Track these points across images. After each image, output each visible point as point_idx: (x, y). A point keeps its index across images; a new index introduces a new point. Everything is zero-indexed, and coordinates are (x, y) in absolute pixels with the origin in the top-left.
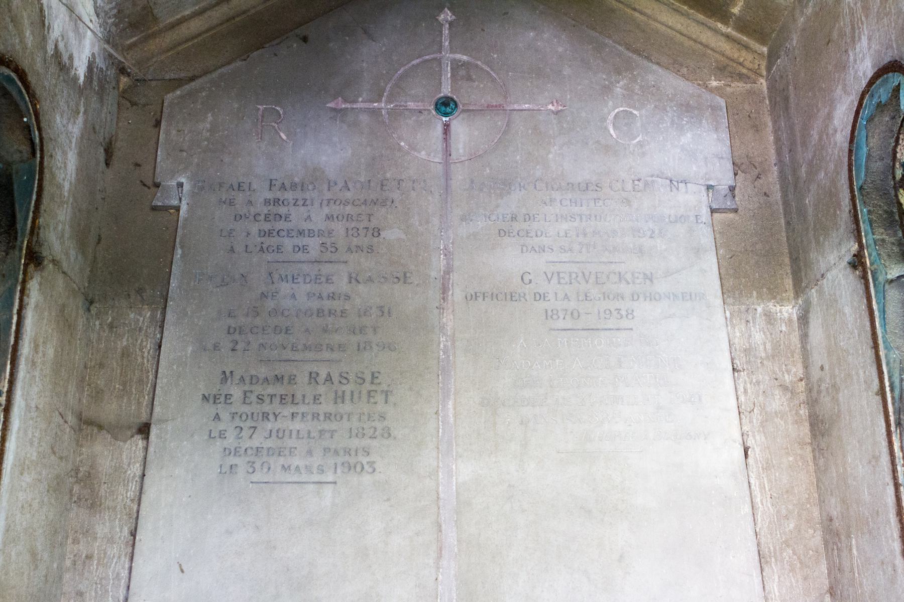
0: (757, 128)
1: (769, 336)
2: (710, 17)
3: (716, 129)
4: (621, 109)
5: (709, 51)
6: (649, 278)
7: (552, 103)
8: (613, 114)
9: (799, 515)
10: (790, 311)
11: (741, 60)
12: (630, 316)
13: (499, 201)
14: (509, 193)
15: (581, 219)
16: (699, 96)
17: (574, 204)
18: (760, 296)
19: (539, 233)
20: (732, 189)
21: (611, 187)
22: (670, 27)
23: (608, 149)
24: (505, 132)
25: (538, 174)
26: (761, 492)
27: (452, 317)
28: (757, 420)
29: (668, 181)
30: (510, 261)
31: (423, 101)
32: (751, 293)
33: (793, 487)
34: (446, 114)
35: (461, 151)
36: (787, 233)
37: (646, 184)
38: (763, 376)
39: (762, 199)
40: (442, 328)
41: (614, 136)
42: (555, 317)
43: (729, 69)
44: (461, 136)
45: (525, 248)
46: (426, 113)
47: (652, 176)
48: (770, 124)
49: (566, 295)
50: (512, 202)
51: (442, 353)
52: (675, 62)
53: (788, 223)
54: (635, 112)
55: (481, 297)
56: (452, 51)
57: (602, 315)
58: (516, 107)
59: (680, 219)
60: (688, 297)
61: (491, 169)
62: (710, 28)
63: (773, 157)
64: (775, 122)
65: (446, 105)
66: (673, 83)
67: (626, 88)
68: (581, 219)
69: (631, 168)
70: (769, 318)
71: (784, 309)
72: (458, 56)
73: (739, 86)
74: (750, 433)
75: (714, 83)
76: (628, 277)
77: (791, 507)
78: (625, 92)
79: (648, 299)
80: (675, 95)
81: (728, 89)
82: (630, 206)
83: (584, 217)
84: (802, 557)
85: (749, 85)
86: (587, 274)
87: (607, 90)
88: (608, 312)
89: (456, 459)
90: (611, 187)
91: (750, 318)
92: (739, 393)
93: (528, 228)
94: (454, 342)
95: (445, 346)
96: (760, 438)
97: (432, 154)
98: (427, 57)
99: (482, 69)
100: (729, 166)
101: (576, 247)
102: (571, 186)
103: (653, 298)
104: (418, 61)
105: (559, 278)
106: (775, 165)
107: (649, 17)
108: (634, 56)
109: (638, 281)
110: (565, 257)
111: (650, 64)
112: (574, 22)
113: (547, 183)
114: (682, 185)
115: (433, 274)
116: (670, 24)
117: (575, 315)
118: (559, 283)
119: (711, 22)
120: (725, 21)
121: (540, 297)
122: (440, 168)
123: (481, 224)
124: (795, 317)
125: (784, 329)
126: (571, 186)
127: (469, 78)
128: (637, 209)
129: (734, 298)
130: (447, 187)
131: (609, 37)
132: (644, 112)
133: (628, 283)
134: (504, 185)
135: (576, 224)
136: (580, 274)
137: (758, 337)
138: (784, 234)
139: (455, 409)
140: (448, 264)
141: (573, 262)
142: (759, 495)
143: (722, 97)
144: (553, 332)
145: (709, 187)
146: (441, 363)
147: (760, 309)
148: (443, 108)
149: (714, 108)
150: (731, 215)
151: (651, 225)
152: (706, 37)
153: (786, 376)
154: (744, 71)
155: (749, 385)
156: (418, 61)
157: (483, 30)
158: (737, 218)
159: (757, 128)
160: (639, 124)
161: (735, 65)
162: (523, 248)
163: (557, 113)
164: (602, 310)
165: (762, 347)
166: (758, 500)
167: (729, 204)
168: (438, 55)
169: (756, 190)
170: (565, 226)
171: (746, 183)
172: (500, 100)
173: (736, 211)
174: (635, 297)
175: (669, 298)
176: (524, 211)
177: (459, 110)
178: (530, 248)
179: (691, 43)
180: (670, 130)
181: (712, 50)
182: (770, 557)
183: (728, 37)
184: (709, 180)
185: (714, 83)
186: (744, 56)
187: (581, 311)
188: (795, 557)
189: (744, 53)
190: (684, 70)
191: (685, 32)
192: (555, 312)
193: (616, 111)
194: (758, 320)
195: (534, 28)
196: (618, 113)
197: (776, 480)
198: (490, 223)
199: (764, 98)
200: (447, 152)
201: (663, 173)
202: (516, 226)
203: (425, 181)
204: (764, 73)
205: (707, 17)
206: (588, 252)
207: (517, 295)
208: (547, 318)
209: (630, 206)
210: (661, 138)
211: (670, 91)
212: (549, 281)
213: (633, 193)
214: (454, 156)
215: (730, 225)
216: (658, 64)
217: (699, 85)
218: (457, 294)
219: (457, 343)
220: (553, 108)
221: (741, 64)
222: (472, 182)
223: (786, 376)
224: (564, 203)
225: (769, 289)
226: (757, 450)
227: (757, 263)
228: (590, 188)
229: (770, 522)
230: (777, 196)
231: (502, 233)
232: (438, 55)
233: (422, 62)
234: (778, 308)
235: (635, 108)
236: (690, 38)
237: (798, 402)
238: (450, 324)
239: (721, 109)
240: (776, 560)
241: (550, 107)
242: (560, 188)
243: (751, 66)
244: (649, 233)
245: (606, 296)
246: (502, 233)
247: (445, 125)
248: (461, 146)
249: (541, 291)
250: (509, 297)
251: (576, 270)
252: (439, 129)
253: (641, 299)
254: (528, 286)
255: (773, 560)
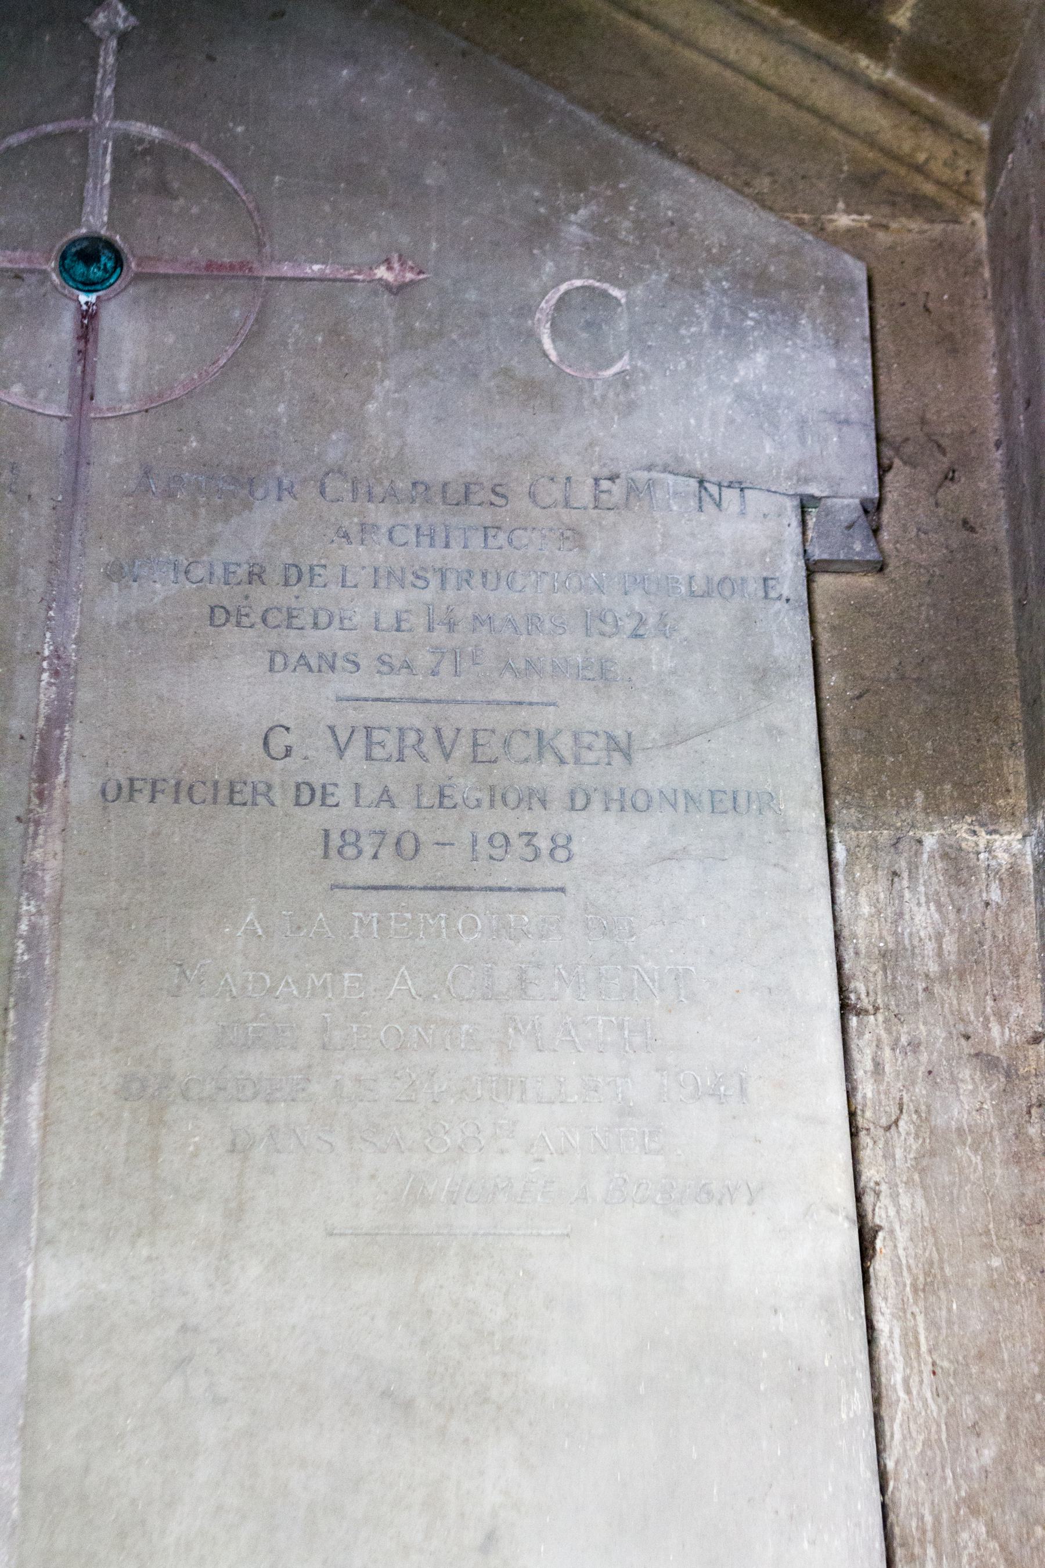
0: (952, 344)
1: (952, 916)
2: (839, 39)
3: (837, 344)
4: (578, 283)
5: (834, 133)
6: (622, 748)
7: (388, 262)
8: (554, 296)
9: (1012, 1422)
10: (1017, 846)
11: (921, 157)
12: (561, 854)
13: (219, 527)
14: (248, 506)
15: (443, 582)
16: (796, 252)
17: (425, 541)
18: (934, 807)
19: (323, 619)
20: (872, 509)
21: (532, 495)
22: (727, 64)
23: (536, 392)
24: (254, 336)
25: (333, 455)
26: (906, 1356)
27: (58, 846)
28: (907, 1149)
29: (693, 483)
30: (236, 693)
31: (26, 246)
32: (910, 798)
33: (997, 1343)
34: (88, 286)
35: (123, 387)
36: (1018, 630)
37: (632, 490)
38: (932, 1030)
39: (958, 538)
40: (29, 878)
41: (553, 356)
42: (350, 851)
43: (886, 181)
44: (127, 345)
45: (279, 659)
46: (33, 279)
47: (649, 468)
48: (991, 333)
49: (386, 790)
50: (257, 530)
51: (21, 946)
52: (740, 159)
53: (1020, 605)
54: (616, 292)
55: (147, 792)
56: (119, 113)
57: (483, 846)
58: (286, 269)
59: (720, 587)
60: (729, 804)
61: (202, 439)
62: (836, 68)
63: (993, 428)
64: (1001, 326)
65: (91, 261)
66: (722, 214)
67: (595, 225)
68: (443, 582)
69: (591, 445)
70: (957, 865)
71: (999, 842)
72: (136, 127)
73: (910, 230)
74: (884, 1187)
75: (844, 220)
76: (565, 744)
77: (988, 1400)
78: (590, 236)
79: (615, 806)
80: (731, 248)
81: (881, 235)
82: (582, 547)
83: (452, 578)
84: (1014, 1545)
85: (938, 229)
86: (448, 734)
87: (541, 230)
88: (499, 841)
89: (37, 1249)
90: (532, 495)
91: (902, 865)
92: (859, 1074)
93: (294, 604)
94: (58, 916)
95: (33, 927)
96: (912, 1202)
97: (42, 394)
98: (50, 128)
99: (198, 163)
100: (866, 443)
101: (424, 659)
102: (423, 492)
103: (630, 803)
104: (23, 137)
105: (369, 744)
106: (998, 444)
107: (675, 36)
108: (624, 140)
109: (591, 757)
110: (391, 685)
111: (667, 163)
112: (464, 44)
113: (354, 482)
114: (730, 496)
115: (17, 724)
116: (732, 56)
117: (405, 847)
118: (369, 757)
119: (841, 52)
120: (878, 54)
121: (312, 794)
122: (60, 430)
123: (161, 588)
124: (1028, 865)
125: (995, 895)
126: (423, 492)
127: (163, 189)
128: (602, 559)
129: (861, 808)
130: (74, 488)
131: (562, 87)
132: (639, 291)
133: (562, 761)
134: (235, 482)
135: (428, 595)
136: (430, 734)
137: (922, 918)
138: (1010, 635)
139: (45, 1105)
140: (61, 697)
141: (413, 700)
142: (900, 1365)
143: (859, 257)
144: (339, 893)
145: (805, 505)
146: (18, 976)
147: (930, 842)
148: (80, 268)
149: (835, 287)
150: (867, 581)
151: (637, 601)
152: (828, 92)
153: (995, 1030)
154: (929, 188)
155: (887, 1053)
156: (23, 137)
157: (211, 58)
158: (883, 589)
159: (952, 344)
160: (623, 326)
161: (902, 171)
162: (276, 660)
163: (397, 290)
164: (482, 836)
165: (930, 947)
166: (897, 1378)
167: (859, 547)
168: (80, 124)
169: (941, 511)
170: (397, 600)
171: (915, 494)
172: (245, 251)
173: (880, 567)
174: (578, 800)
175: (674, 806)
176: (285, 555)
177: (126, 277)
178: (294, 658)
179: (789, 109)
180: (708, 343)
181: (844, 128)
182: (922, 1543)
183: (884, 93)
184: (807, 481)
185: (844, 220)
186: (932, 149)
187: (422, 838)
188: (993, 1545)
189: (928, 139)
190: (764, 183)
191: (772, 79)
192: (351, 838)
193: (564, 287)
194: (924, 872)
195: (351, 57)
196: (567, 293)
197: (950, 1323)
198: (188, 586)
199: (979, 262)
200: (83, 390)
201: (679, 460)
202: (263, 597)
203: (13, 467)
204: (982, 195)
205: (831, 38)
206: (456, 674)
207: (249, 789)
208: (326, 856)
209: (582, 547)
210: (682, 365)
211: (716, 238)
212: (341, 752)
213: (595, 513)
214: (102, 399)
215: (862, 605)
216: (692, 164)
217: (800, 223)
218: (78, 783)
219: (68, 920)
220: (389, 276)
221: (919, 169)
222: (147, 473)
223: (995, 1030)
224: (399, 536)
225: (958, 785)
226: (902, 1236)
227: (930, 712)
228: (475, 499)
229: (927, 1443)
230: (998, 531)
231: (220, 616)
232: (80, 124)
233: (33, 141)
234: (983, 838)
235: (615, 281)
236: (784, 96)
237: (1023, 1102)
238: (53, 864)
239: (853, 288)
240: (939, 1556)
241: (381, 272)
242: (391, 495)
243: (946, 175)
244: (629, 625)
245: (497, 797)
246: (220, 615)
247: (84, 315)
248: (123, 373)
249: (317, 779)
250: (224, 793)
251: (417, 723)
252: (67, 324)
253: (597, 805)
254: (279, 765)
255: (931, 1551)
